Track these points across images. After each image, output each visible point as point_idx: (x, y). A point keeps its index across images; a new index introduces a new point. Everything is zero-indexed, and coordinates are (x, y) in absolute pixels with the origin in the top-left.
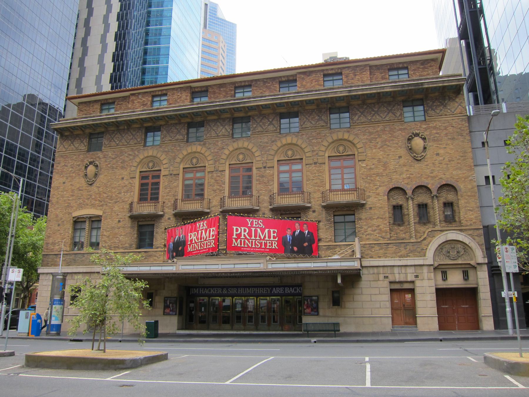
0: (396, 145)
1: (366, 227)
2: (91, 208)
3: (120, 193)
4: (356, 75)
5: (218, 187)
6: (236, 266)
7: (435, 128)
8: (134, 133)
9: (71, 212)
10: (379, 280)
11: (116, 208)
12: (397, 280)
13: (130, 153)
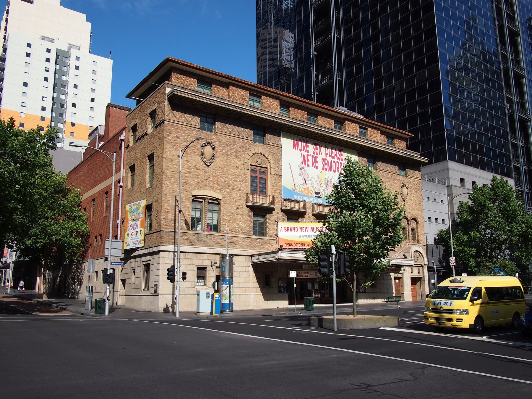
2: (210, 190)
3: (236, 181)
9: (189, 189)
11: (234, 195)
13: (242, 144)
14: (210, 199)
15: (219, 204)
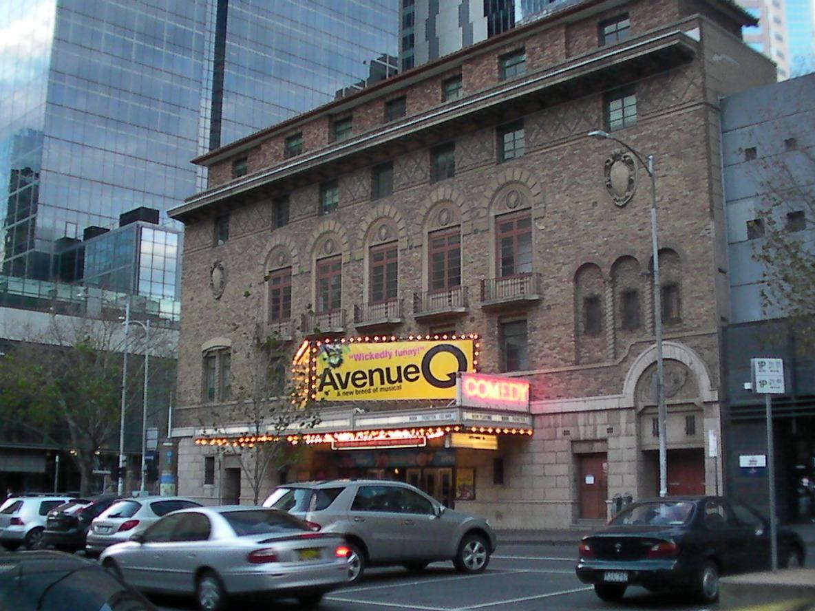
1: (541, 343)
7: (651, 138)
10: (556, 438)
12: (582, 439)
13: (257, 243)
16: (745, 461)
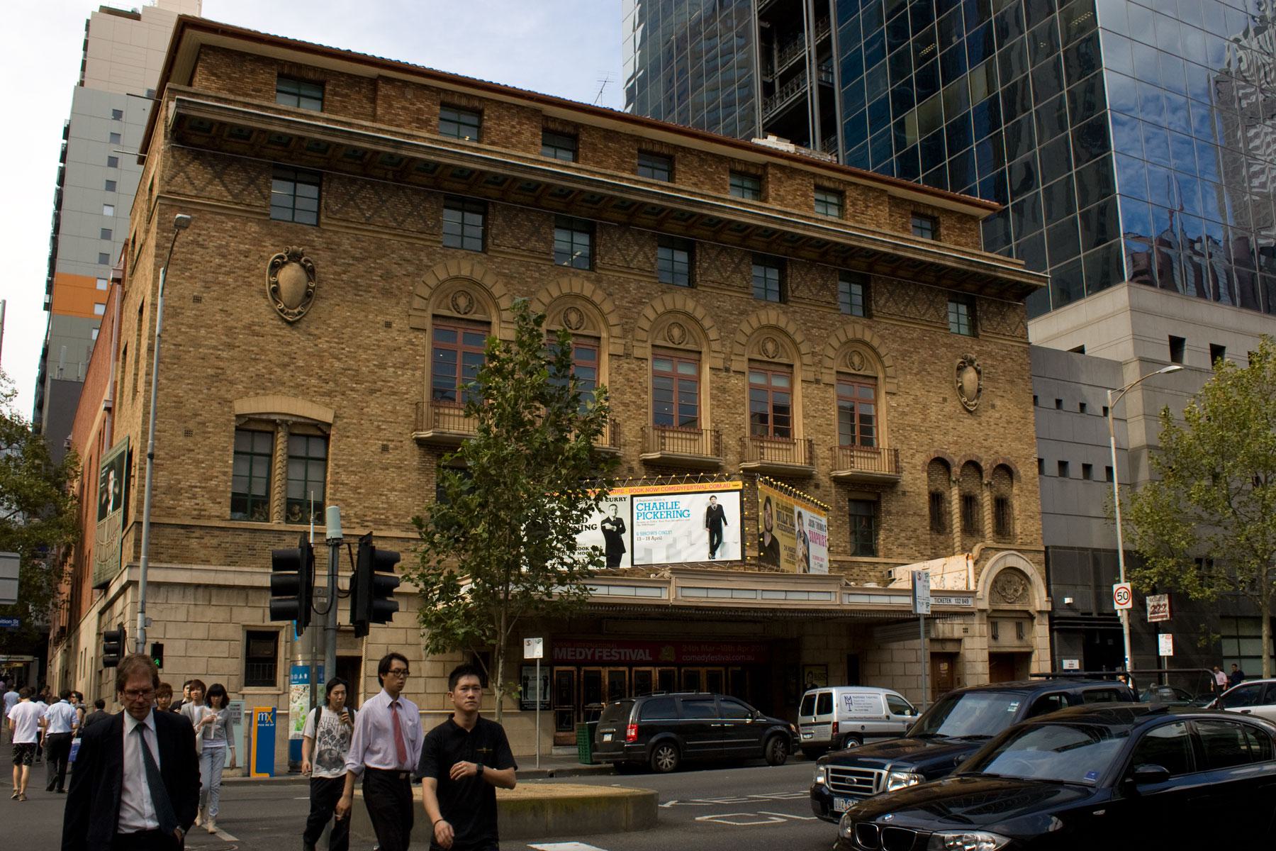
0: (938, 374)
2: (295, 396)
3: (382, 366)
4: (867, 207)
5: (633, 398)
6: (791, 596)
7: (990, 354)
8: (416, 200)
9: (229, 396)
11: (373, 409)
13: (407, 255)
14: (295, 423)
15: (326, 438)
16: (1067, 664)
